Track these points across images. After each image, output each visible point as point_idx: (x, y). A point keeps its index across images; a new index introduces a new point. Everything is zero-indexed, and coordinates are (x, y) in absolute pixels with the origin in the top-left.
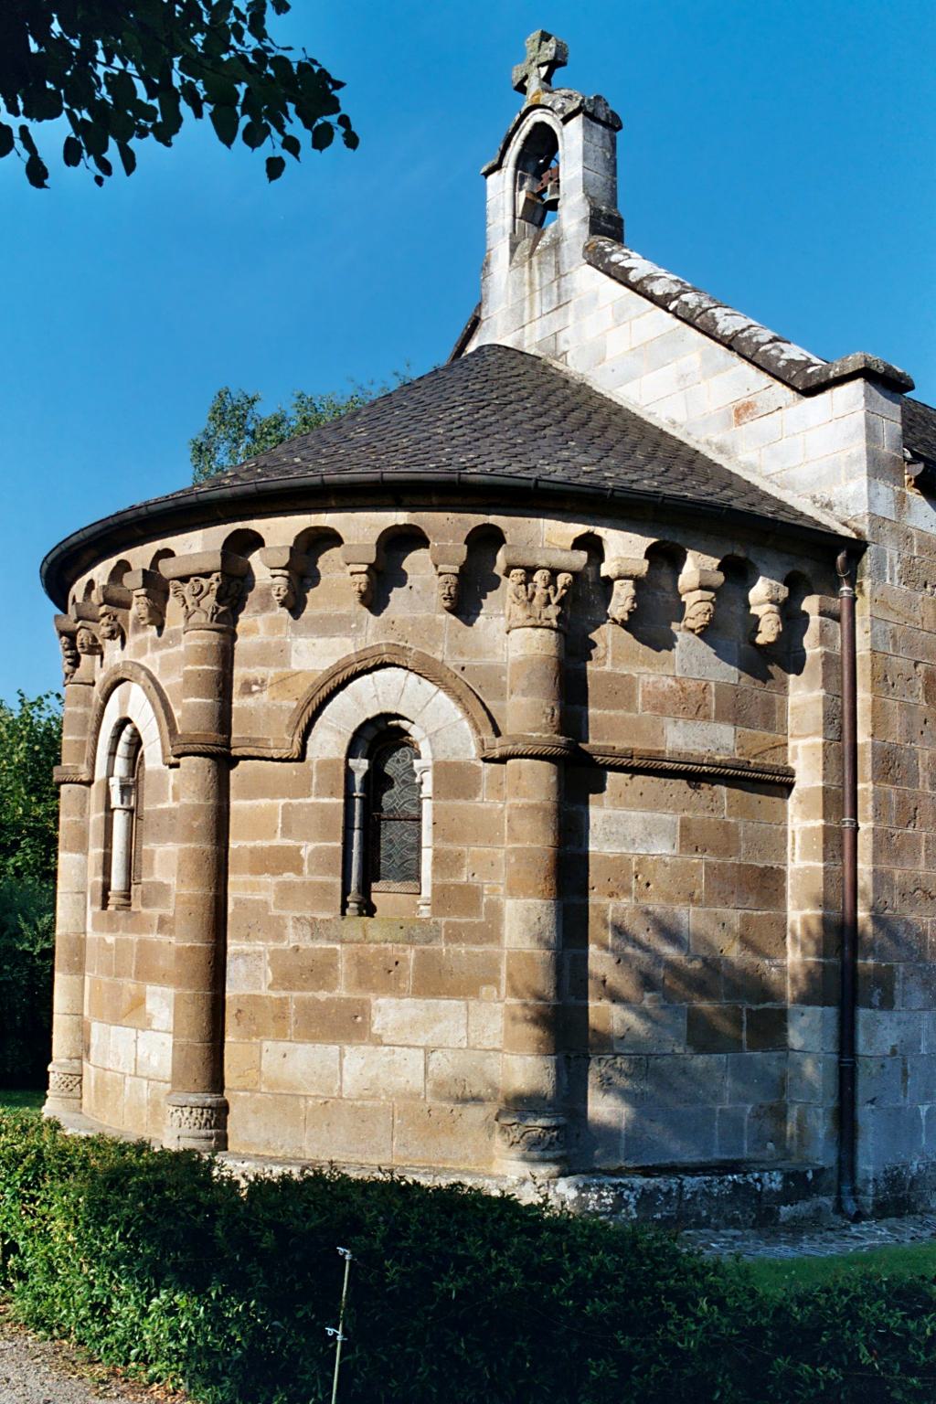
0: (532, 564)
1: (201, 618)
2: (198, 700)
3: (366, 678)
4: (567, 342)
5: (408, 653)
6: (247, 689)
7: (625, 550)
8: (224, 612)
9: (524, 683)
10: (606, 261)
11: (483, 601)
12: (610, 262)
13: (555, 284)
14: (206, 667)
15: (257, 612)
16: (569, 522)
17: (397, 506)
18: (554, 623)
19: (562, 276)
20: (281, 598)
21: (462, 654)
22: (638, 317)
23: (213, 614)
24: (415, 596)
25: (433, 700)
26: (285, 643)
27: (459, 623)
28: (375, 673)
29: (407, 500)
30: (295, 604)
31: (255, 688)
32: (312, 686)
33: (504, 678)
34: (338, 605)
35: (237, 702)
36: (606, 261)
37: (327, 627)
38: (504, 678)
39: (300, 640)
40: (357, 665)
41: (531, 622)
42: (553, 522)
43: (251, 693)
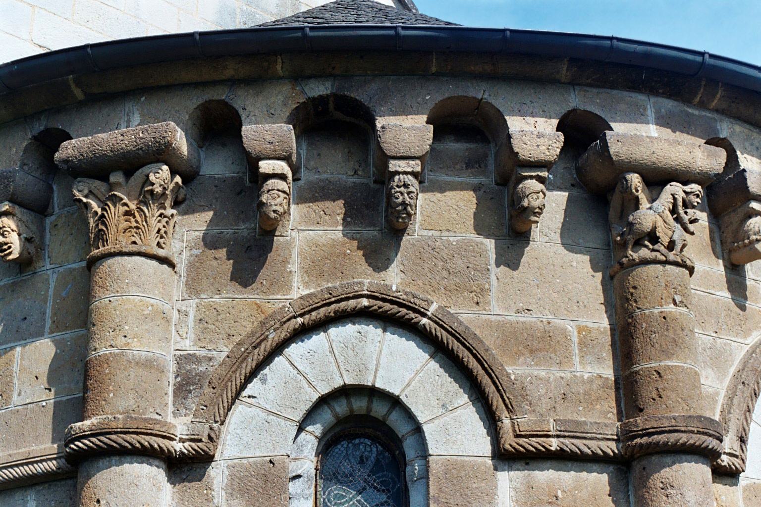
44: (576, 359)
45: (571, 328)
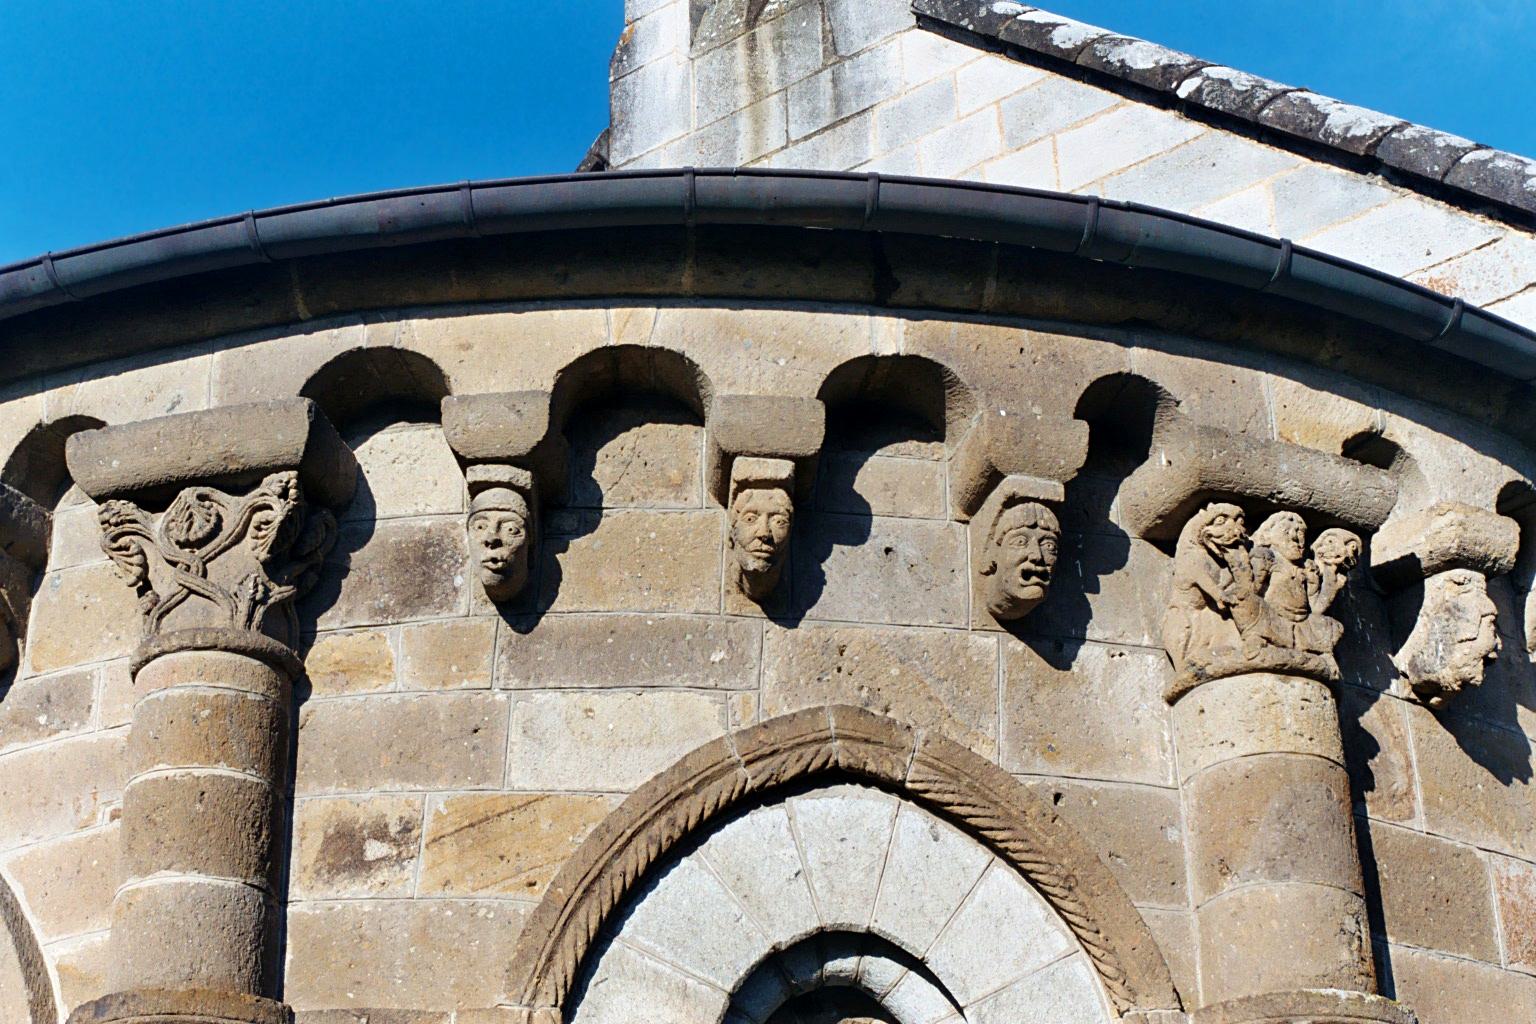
0: (1263, 492)
1: (224, 618)
2: (193, 878)
3: (764, 817)
5: (905, 738)
6: (347, 851)
8: (281, 603)
9: (1268, 837)
10: (983, 12)
12: (990, 13)
13: (827, 74)
14: (223, 770)
15: (384, 611)
16: (1321, 388)
17: (880, 301)
18: (1332, 666)
19: (843, 58)
20: (502, 552)
21: (1051, 752)
22: (1076, 126)
23: (255, 603)
24: (904, 578)
25: (980, 892)
26: (491, 708)
27: (1037, 662)
28: (794, 802)
29: (910, 288)
30: (523, 592)
31: (374, 850)
32: (597, 835)
33: (1172, 835)
34: (667, 592)
35: (304, 900)
36: (983, 12)
37: (625, 658)
38: (1172, 835)
39: (539, 697)
40: (743, 772)
41: (1272, 656)
42: (1291, 385)
43: (360, 865)
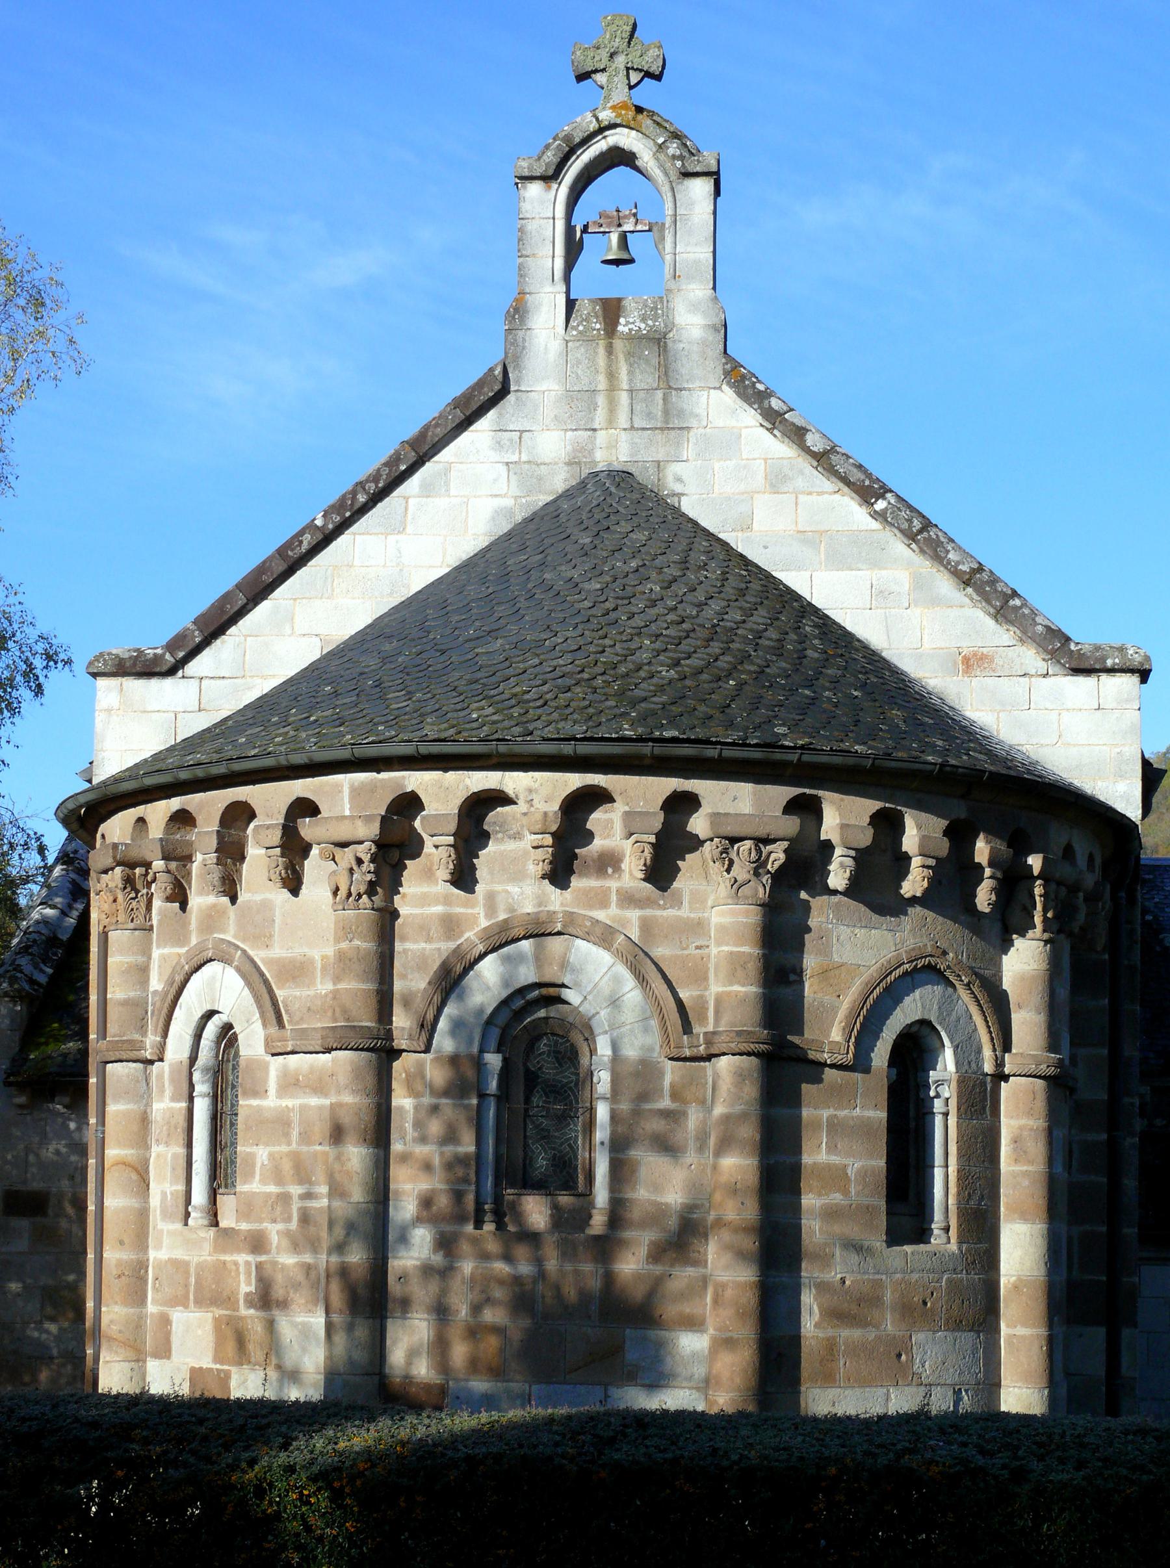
4: (679, 480)
7: (843, 818)
11: (475, 861)
44: (319, 980)
45: (317, 958)
